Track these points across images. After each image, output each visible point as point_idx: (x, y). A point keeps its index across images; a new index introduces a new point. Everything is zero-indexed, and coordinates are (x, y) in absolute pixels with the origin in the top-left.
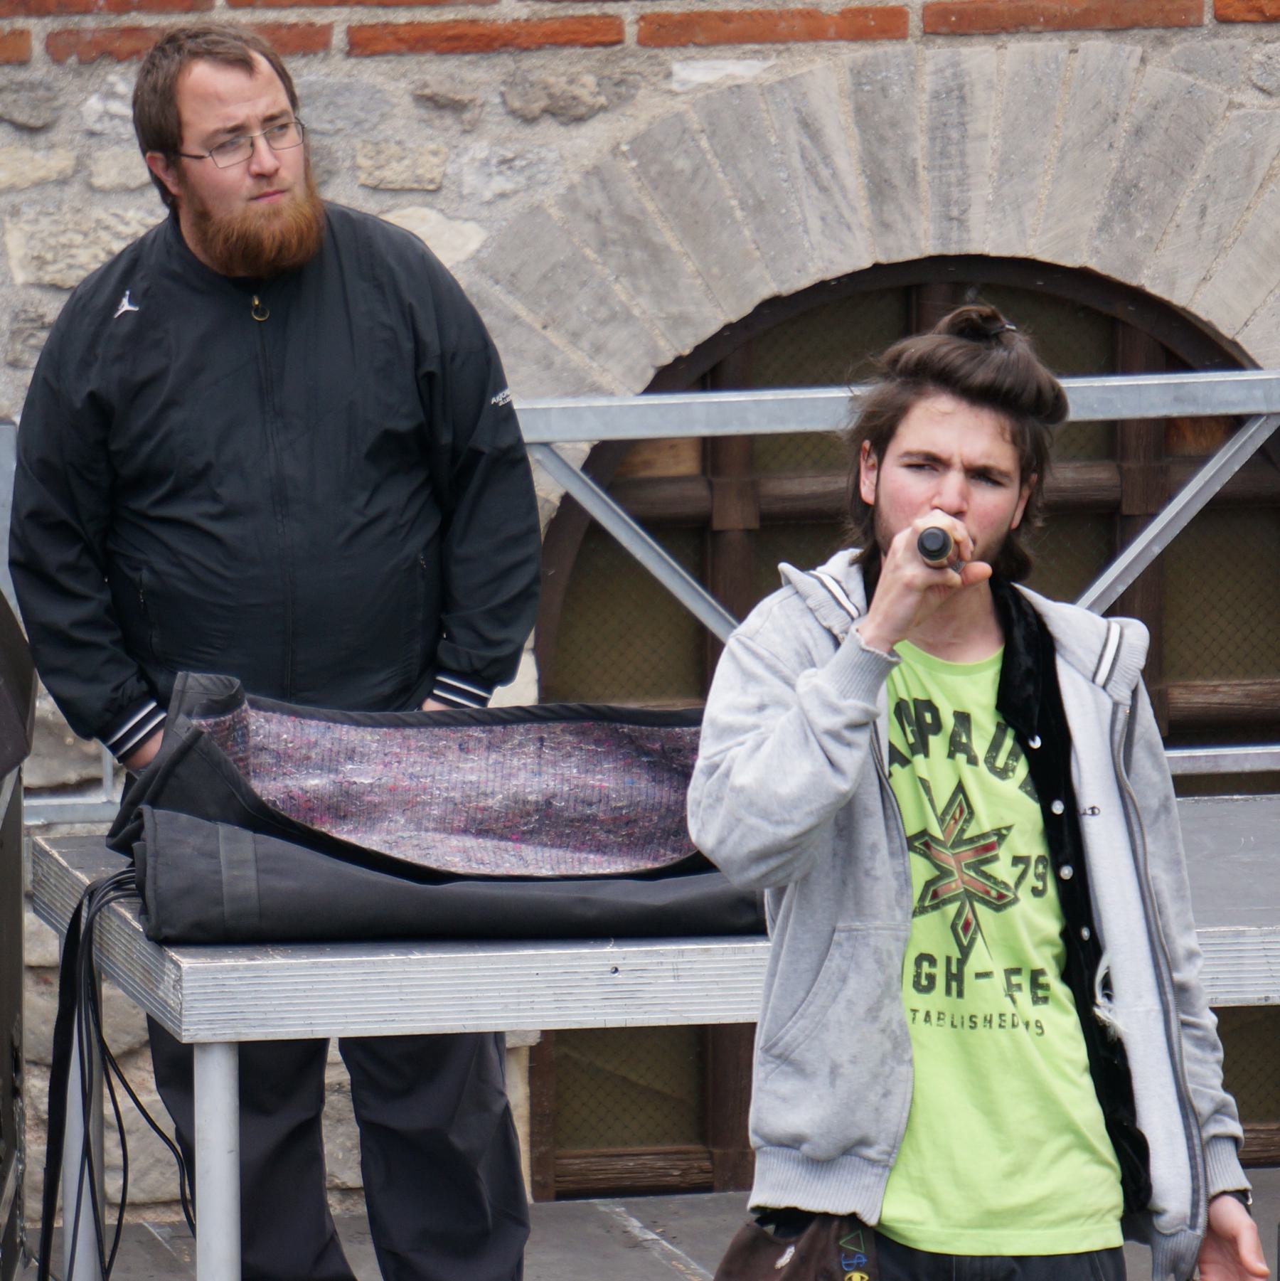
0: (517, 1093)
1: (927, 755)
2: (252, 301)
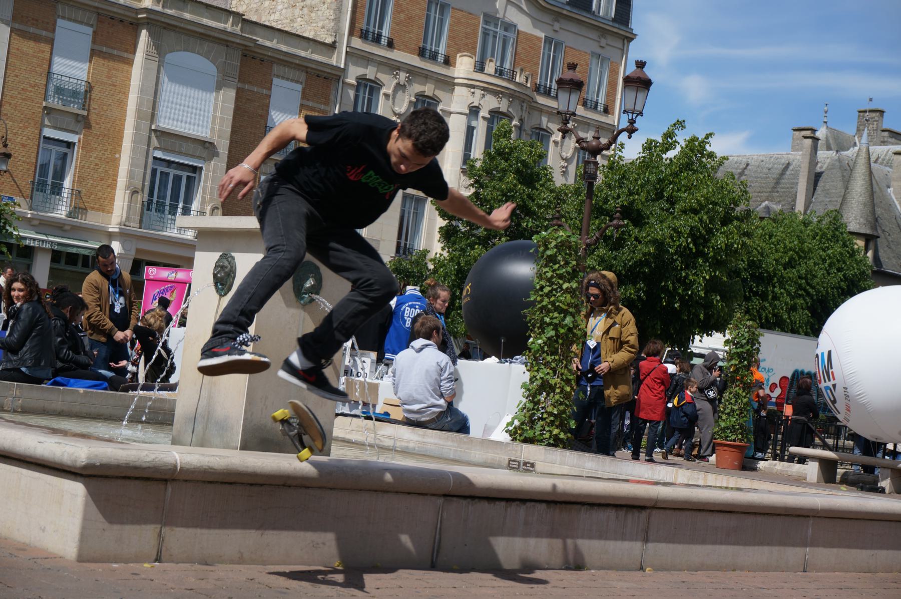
0: (167, 208)
1: (630, 137)
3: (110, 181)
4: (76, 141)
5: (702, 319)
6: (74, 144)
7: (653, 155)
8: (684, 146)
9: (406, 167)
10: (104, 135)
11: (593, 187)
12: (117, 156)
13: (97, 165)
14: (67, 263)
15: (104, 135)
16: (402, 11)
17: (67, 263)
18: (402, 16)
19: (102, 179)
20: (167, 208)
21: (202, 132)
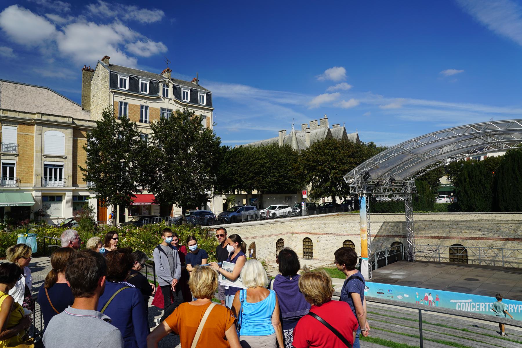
0: (53, 179)
2: (67, 277)
3: (30, 173)
4: (16, 163)
5: (245, 193)
6: (15, 163)
7: (241, 177)
8: (327, 197)
9: (348, 206)
10: (26, 159)
11: (292, 194)
12: (32, 165)
13: (25, 169)
14: (79, 200)
15: (26, 159)
16: (132, 110)
17: (79, 200)
18: (132, 111)
19: (27, 173)
20: (53, 179)
21: (62, 154)
